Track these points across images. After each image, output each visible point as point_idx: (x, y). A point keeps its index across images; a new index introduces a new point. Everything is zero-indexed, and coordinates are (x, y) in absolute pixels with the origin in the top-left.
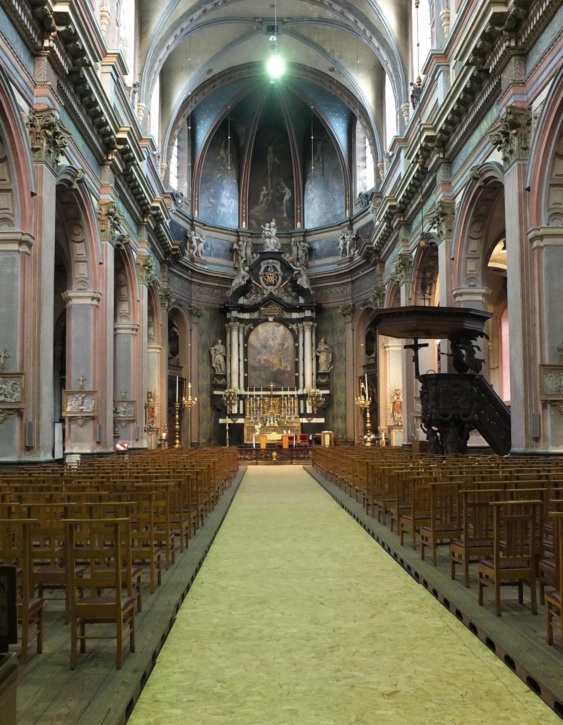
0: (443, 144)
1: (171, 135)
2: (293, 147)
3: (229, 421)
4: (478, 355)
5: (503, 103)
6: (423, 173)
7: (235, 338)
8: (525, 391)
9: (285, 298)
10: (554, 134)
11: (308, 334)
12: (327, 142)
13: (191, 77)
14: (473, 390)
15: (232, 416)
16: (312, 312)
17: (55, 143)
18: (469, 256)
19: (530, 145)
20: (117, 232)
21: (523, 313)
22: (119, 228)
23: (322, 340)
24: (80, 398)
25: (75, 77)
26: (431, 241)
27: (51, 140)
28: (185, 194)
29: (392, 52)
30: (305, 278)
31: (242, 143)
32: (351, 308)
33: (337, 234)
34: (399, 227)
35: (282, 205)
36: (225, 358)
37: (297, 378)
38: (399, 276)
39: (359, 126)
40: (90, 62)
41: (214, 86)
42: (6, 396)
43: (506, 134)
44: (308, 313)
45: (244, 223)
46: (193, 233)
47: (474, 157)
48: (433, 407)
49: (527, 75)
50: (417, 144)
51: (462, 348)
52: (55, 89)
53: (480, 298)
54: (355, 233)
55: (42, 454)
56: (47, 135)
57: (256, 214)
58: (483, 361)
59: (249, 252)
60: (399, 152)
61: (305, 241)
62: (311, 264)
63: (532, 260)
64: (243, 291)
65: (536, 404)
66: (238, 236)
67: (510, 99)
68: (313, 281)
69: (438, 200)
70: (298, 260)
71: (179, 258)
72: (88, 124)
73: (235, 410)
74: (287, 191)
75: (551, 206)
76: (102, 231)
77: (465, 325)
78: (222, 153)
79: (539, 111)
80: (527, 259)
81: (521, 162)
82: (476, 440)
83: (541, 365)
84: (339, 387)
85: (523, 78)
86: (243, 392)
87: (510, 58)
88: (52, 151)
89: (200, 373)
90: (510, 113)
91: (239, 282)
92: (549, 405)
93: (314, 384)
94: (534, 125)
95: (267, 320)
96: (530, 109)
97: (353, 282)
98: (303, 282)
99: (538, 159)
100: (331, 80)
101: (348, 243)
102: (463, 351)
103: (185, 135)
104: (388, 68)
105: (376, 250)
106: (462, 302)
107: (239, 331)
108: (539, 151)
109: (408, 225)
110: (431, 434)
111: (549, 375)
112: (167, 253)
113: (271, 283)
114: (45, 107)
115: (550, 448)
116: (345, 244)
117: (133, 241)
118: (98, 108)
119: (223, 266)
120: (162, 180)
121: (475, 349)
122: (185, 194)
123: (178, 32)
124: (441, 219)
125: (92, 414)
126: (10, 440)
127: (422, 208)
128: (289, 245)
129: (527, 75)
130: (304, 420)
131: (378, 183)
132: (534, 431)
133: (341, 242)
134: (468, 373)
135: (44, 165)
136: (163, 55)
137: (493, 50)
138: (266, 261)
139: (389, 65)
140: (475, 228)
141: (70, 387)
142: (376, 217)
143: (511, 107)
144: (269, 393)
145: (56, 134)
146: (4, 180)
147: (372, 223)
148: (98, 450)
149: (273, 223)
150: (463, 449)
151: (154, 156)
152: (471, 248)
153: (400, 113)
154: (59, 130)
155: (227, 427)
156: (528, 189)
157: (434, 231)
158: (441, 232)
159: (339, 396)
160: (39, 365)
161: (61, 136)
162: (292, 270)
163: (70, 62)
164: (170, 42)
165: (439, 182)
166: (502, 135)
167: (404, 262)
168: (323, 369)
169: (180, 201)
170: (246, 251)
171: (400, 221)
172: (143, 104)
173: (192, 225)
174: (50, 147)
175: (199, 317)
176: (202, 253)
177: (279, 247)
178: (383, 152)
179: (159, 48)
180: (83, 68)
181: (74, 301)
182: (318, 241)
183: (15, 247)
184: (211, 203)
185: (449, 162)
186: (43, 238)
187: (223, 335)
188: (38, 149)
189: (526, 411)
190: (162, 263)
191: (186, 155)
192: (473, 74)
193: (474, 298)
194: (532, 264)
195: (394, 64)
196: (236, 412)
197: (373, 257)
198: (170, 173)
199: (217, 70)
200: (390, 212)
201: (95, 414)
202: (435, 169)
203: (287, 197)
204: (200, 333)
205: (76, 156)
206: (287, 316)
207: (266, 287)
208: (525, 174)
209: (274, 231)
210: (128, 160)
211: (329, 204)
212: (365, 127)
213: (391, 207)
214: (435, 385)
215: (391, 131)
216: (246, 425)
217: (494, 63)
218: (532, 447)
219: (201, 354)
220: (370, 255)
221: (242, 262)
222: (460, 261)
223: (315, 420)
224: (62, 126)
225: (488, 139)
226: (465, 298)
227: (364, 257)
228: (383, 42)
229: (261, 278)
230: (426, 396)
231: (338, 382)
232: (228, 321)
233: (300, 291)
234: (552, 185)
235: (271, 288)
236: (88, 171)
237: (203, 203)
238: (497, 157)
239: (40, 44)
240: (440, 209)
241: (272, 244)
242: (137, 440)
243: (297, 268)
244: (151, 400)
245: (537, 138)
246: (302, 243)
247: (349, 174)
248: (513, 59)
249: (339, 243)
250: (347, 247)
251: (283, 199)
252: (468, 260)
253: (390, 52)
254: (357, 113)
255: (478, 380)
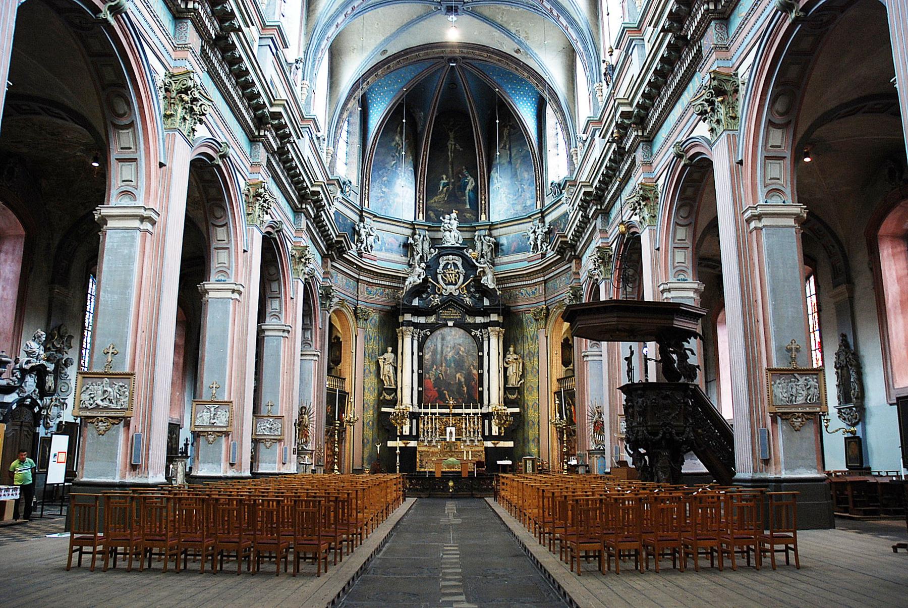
0: (641, 121)
1: (339, 117)
2: (477, 130)
3: (398, 444)
4: (693, 360)
5: (705, 70)
6: (620, 154)
7: (408, 344)
8: (750, 401)
9: (468, 299)
10: (766, 99)
11: (494, 341)
12: (515, 128)
13: (364, 58)
14: (687, 404)
15: (403, 437)
16: (499, 315)
17: (192, 110)
18: (676, 245)
19: (739, 115)
20: (267, 218)
21: (743, 306)
22: (269, 211)
23: (511, 349)
24: (212, 409)
25: (222, 43)
26: (632, 230)
27: (187, 106)
28: (354, 183)
29: (582, 31)
30: (490, 276)
31: (420, 128)
32: (544, 311)
33: (527, 227)
34: (595, 216)
35: (465, 195)
36: (396, 369)
37: (481, 393)
38: (596, 272)
39: (549, 111)
40: (240, 26)
41: (388, 68)
42: (111, 402)
43: (711, 103)
44: (494, 317)
45: (421, 215)
46: (362, 225)
47: (677, 132)
48: (639, 423)
49: (730, 39)
50: (611, 121)
51: (673, 353)
52: (198, 52)
53: (691, 294)
54: (547, 226)
55: (151, 474)
56: (182, 100)
57: (434, 205)
58: (698, 367)
59: (426, 246)
60: (593, 135)
61: (490, 235)
62: (497, 261)
63: (750, 243)
64: (419, 290)
65: (764, 418)
66: (414, 229)
67: (712, 64)
68: (499, 281)
69: (639, 182)
70: (482, 256)
71: (344, 252)
72: (238, 94)
73: (406, 430)
74: (471, 180)
75: (768, 182)
76: (249, 214)
77: (675, 322)
78: (397, 138)
79: (747, 76)
80: (744, 242)
81: (731, 133)
82: (694, 465)
83: (769, 370)
84: (530, 404)
85: (726, 43)
86: (417, 410)
87: (710, 22)
88: (188, 118)
89: (366, 387)
90: (714, 79)
91: (414, 279)
92: (779, 418)
93: (502, 399)
94: (742, 90)
95: (446, 325)
96: (736, 75)
97: (545, 282)
98: (489, 281)
99: (749, 128)
100: (517, 62)
101: (540, 237)
102: (674, 356)
103: (356, 119)
104: (579, 47)
105: (571, 244)
106: (671, 297)
107: (413, 336)
108: (750, 119)
109: (606, 213)
110: (637, 457)
111: (778, 381)
112: (329, 246)
113: (451, 285)
114: (182, 71)
115: (783, 473)
116: (536, 239)
117: (288, 230)
118: (248, 77)
119: (397, 262)
120: (327, 166)
121: (688, 352)
122: (354, 183)
123: (349, 10)
124: (643, 203)
125: (225, 429)
126: (113, 456)
127: (620, 195)
128: (473, 239)
129: (730, 39)
130: (489, 444)
131: (571, 172)
132: (763, 451)
133: (532, 236)
134: (681, 381)
135: (177, 133)
136: (332, 32)
137: (690, 14)
138: (445, 258)
139: (579, 44)
140: (683, 213)
141: (201, 396)
142: (567, 207)
143: (714, 71)
144: (447, 411)
145: (195, 100)
146: (130, 148)
147: (566, 214)
148: (230, 473)
149: (454, 215)
150: (677, 477)
151: (318, 138)
152: (678, 237)
153: (593, 94)
154: (197, 95)
155: (398, 451)
156: (741, 163)
157: (636, 218)
158: (643, 218)
159: (531, 414)
160: (154, 364)
161: (200, 103)
162: (476, 268)
163: (209, 10)
164: (340, 19)
165: (638, 162)
166: (706, 104)
167: (603, 257)
168: (513, 382)
169: (347, 189)
170: (423, 247)
171: (596, 209)
172: (307, 83)
173: (361, 216)
174: (186, 113)
175: (366, 320)
176: (371, 247)
177: (461, 242)
178: (576, 137)
179: (328, 25)
180: (232, 34)
181: (212, 294)
182: (506, 236)
183: (136, 223)
184: (383, 192)
185: (649, 141)
186: (170, 214)
187: (391, 342)
188: (172, 115)
189: (752, 427)
190: (324, 257)
191: (356, 140)
192: (670, 41)
193: (686, 292)
194: (751, 250)
195: (584, 42)
196: (408, 433)
197: (569, 251)
198: (334, 154)
199: (392, 50)
200: (585, 199)
201: (229, 429)
202: (633, 149)
203: (469, 187)
204: (367, 339)
205: (222, 126)
206: (469, 320)
207: (445, 287)
208: (736, 146)
209: (455, 224)
210: (284, 137)
211: (518, 194)
212: (555, 111)
213: (585, 193)
214: (641, 396)
215: (584, 111)
216: (419, 449)
217: (692, 29)
218: (761, 471)
219: (367, 363)
220: (565, 249)
221: (417, 258)
222: (667, 251)
223: (502, 444)
224: (203, 92)
225: (692, 110)
226: (673, 294)
227: (558, 253)
228: (572, 22)
229: (439, 276)
230: (630, 410)
231: (530, 398)
232: (399, 325)
233: (484, 291)
234: (767, 158)
235: (451, 289)
236: (235, 147)
237: (375, 192)
238: (703, 129)
239: (183, 6)
240: (641, 192)
241: (452, 236)
242: (284, 464)
243: (482, 265)
244: (306, 416)
245: (747, 105)
246: (487, 238)
247: (539, 163)
248: (713, 24)
249: (529, 239)
250: (539, 242)
251: (465, 189)
252: (676, 250)
253: (579, 31)
254: (547, 96)
255: (692, 390)
